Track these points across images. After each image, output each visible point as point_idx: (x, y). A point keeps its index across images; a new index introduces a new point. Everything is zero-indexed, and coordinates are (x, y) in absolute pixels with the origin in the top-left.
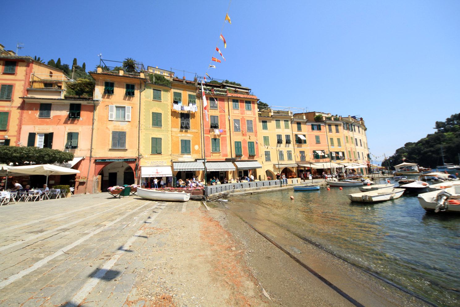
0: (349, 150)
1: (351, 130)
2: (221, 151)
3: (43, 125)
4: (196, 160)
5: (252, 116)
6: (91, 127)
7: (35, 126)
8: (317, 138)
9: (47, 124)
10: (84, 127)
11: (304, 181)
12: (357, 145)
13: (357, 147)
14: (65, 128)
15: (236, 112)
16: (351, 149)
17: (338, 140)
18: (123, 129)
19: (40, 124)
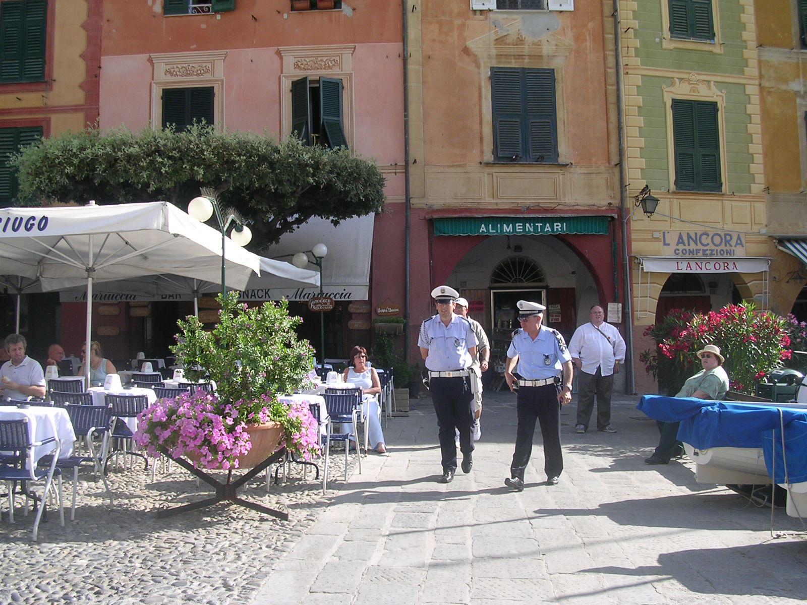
7: (281, 48)
14: (281, 58)
19: (174, 47)
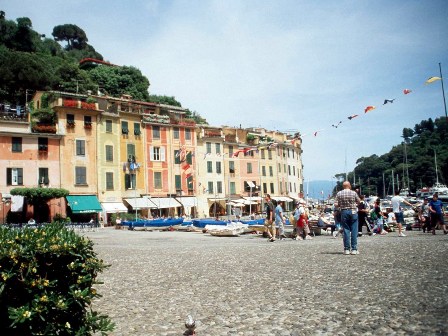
0: (281, 180)
1: (36, 127)
2: (162, 186)
3: (17, 159)
4: (141, 196)
5: (191, 146)
6: (58, 162)
8: (249, 165)
9: (21, 158)
10: (52, 162)
11: (350, 244)
12: (290, 174)
13: (289, 176)
15: (177, 141)
16: (283, 181)
17: (230, 164)
18: (83, 164)
19: (14, 159)
